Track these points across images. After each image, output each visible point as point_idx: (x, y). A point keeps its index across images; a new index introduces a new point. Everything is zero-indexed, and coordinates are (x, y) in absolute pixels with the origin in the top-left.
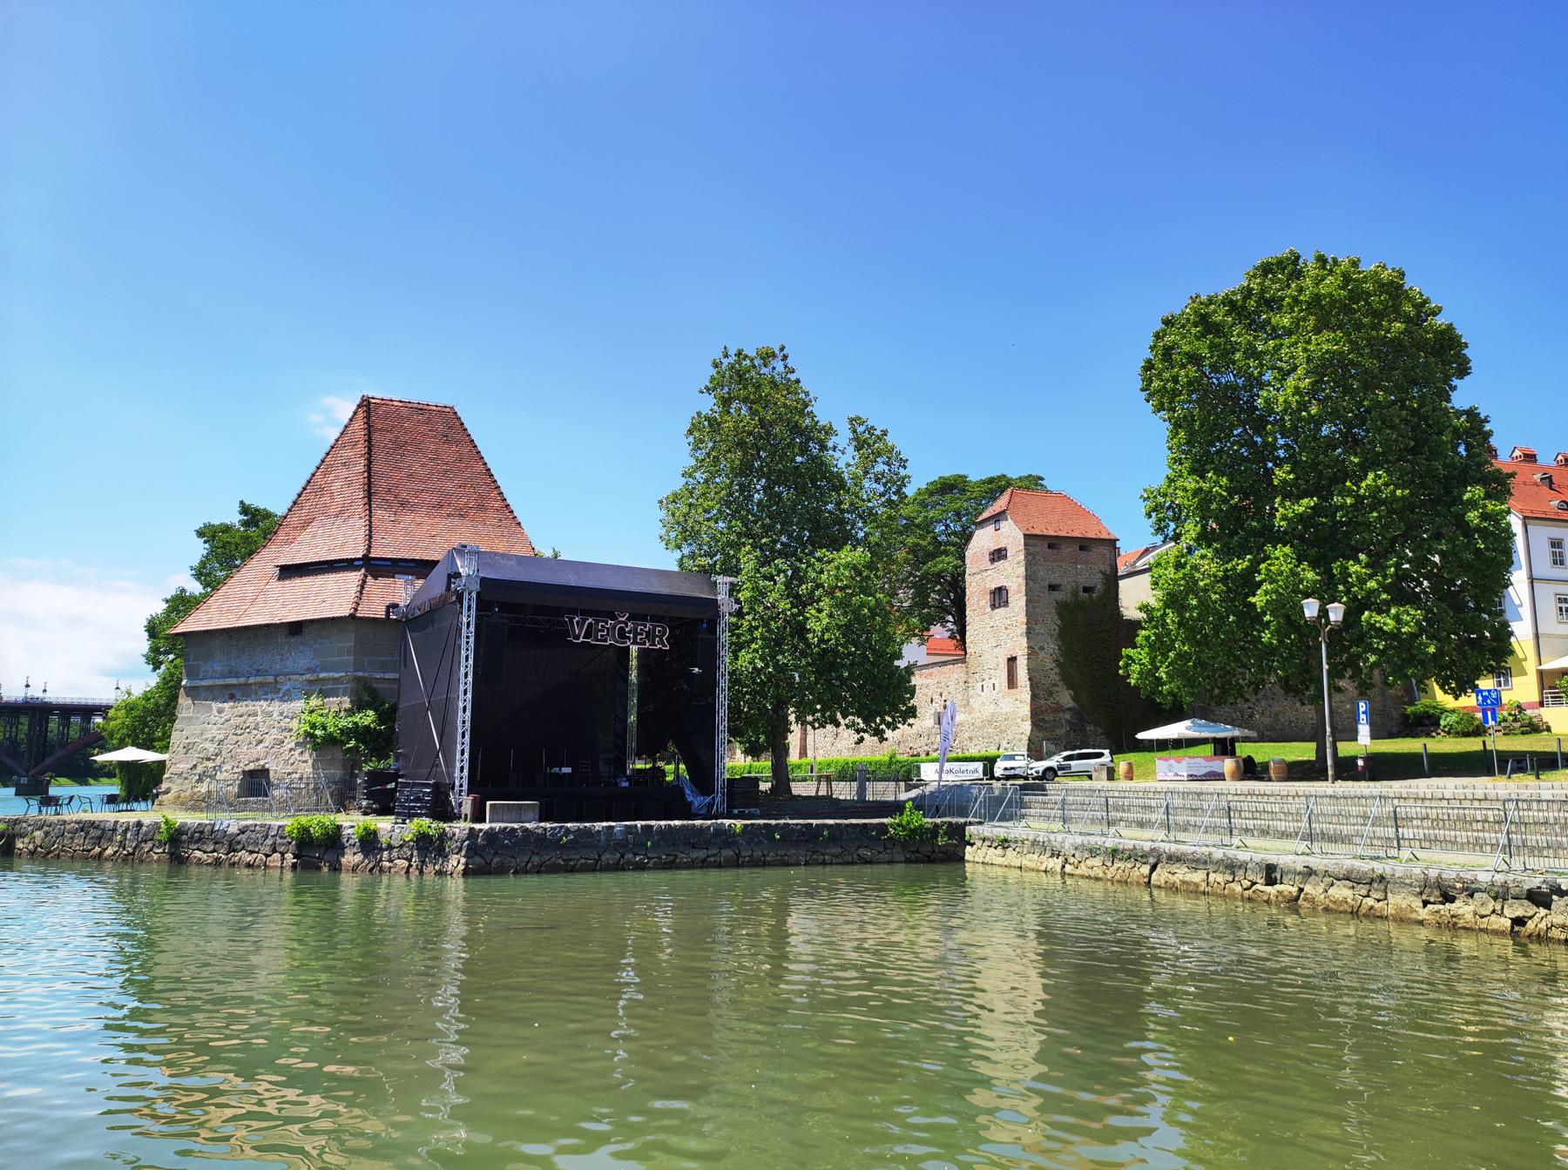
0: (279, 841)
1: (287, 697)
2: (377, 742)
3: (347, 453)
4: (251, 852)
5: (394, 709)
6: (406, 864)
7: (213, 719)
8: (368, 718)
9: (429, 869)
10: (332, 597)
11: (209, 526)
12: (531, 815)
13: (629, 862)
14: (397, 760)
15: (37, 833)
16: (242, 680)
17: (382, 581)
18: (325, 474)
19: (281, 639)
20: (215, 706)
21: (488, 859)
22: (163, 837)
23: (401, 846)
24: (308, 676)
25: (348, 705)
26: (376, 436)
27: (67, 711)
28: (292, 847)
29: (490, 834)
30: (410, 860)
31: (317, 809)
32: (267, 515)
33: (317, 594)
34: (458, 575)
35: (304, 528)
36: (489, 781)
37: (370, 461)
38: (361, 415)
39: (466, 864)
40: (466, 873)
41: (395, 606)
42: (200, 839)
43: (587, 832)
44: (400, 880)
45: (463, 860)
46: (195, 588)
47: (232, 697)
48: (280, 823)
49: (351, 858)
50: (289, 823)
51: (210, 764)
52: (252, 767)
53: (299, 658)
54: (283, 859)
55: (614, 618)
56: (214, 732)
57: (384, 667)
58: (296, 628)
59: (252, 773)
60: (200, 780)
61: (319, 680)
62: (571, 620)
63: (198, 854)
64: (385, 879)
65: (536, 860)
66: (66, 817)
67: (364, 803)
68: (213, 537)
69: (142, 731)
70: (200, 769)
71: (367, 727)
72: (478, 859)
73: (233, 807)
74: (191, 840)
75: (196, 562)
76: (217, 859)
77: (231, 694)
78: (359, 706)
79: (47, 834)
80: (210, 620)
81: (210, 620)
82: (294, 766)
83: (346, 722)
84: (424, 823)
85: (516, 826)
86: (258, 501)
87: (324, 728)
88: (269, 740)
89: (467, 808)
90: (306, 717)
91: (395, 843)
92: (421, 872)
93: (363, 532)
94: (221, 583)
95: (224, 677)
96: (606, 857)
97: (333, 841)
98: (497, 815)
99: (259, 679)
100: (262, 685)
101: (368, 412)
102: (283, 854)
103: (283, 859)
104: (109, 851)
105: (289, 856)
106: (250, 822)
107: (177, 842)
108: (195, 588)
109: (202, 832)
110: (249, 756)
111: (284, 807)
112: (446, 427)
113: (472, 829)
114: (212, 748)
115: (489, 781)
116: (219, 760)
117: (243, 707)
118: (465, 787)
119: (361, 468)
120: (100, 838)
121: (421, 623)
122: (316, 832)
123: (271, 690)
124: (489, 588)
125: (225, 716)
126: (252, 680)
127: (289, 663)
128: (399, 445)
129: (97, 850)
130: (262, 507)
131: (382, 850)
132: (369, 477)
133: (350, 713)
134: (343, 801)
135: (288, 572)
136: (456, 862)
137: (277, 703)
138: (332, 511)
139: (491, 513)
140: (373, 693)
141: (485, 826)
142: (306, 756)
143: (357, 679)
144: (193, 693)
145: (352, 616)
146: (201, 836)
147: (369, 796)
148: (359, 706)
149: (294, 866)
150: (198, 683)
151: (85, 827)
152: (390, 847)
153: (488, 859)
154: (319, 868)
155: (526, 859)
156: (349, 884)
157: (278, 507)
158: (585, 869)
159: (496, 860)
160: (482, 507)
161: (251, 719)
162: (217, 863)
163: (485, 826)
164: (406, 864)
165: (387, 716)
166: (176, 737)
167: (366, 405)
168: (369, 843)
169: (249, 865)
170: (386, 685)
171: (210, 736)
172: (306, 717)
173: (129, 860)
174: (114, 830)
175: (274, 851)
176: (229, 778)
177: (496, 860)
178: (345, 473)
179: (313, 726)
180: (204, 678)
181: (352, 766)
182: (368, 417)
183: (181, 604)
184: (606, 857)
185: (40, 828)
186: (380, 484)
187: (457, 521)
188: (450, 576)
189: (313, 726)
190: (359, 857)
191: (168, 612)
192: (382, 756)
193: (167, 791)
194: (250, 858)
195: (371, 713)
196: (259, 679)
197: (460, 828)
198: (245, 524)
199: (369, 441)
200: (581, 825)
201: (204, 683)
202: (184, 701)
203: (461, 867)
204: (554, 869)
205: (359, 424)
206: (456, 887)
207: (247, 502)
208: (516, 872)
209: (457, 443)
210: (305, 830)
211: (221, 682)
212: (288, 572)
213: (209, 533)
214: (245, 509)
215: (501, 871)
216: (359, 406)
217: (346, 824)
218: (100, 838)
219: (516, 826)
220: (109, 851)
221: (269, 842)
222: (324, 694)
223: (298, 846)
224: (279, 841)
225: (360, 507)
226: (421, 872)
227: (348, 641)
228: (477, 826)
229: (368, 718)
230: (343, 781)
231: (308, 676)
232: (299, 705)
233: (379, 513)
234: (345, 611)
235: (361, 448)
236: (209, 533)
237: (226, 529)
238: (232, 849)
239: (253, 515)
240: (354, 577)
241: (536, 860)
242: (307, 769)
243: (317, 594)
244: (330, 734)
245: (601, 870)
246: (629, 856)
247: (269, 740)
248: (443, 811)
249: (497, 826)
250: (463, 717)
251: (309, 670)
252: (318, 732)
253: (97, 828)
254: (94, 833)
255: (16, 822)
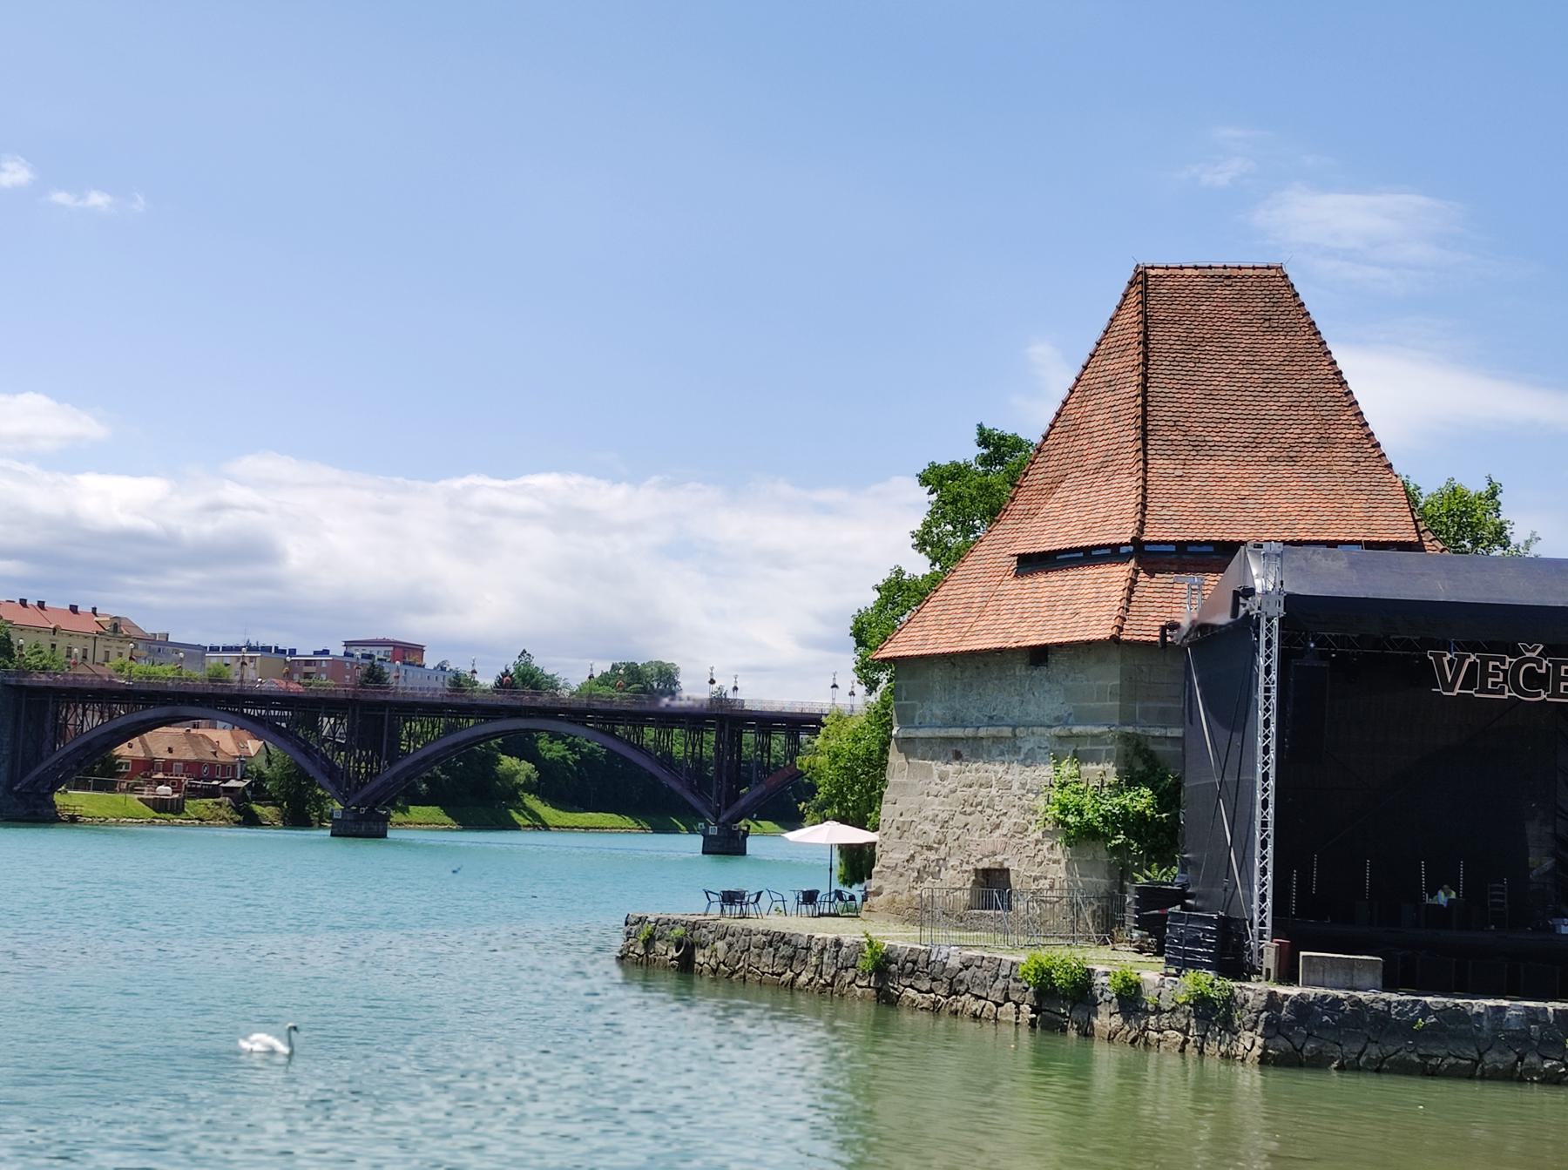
0: (1012, 984)
1: (1029, 760)
2: (1157, 837)
3: (1113, 365)
4: (978, 998)
5: (1178, 784)
6: (1181, 1038)
7: (934, 789)
8: (1141, 800)
9: (1212, 1048)
10: (1086, 607)
11: (934, 467)
12: (1368, 979)
13: (1532, 1070)
14: (1183, 870)
15: (719, 944)
16: (969, 732)
17: (1162, 579)
18: (1081, 402)
19: (1020, 670)
20: (937, 767)
21: (1298, 1042)
22: (865, 964)
23: (1173, 1010)
24: (1057, 730)
25: (1112, 778)
26: (1156, 334)
27: (767, 722)
28: (1030, 996)
29: (1300, 1005)
30: (1186, 1033)
31: (1071, 939)
32: (1018, 444)
33: (1067, 602)
34: (1249, 592)
35: (1052, 491)
36: (1307, 921)
37: (1146, 378)
38: (1134, 299)
39: (1265, 1048)
40: (1264, 1060)
41: (1174, 626)
42: (913, 972)
43: (1459, 1015)
44: (1173, 1060)
45: (1259, 1041)
46: (919, 566)
47: (958, 756)
48: (1014, 959)
49: (1106, 1020)
50: (1020, 955)
51: (932, 856)
52: (985, 864)
53: (1045, 700)
54: (1018, 1012)
55: (1515, 652)
56: (934, 807)
57: (1164, 718)
58: (1039, 655)
59: (986, 872)
60: (919, 879)
61: (1071, 736)
62: (1439, 658)
63: (911, 993)
64: (1153, 1055)
65: (1374, 1051)
66: (751, 924)
67: (1136, 934)
68: (941, 485)
69: (851, 789)
70: (919, 863)
71: (1141, 814)
72: (1282, 1042)
73: (961, 922)
74: (901, 971)
75: (917, 526)
76: (935, 1003)
77: (956, 750)
78: (1131, 779)
79: (730, 946)
80: (925, 639)
81: (925, 639)
82: (1044, 869)
83: (1112, 804)
84: (1202, 980)
85: (1341, 994)
86: (1004, 425)
87: (1080, 814)
88: (1007, 823)
89: (1270, 961)
90: (1056, 795)
91: (1165, 1005)
92: (1201, 1052)
93: (1134, 497)
94: (959, 556)
95: (946, 725)
96: (1491, 1058)
97: (1081, 992)
98: (1318, 974)
99: (992, 731)
100: (997, 739)
101: (1145, 293)
102: (1017, 1005)
103: (1018, 1012)
104: (803, 979)
105: (1025, 1008)
106: (976, 953)
107: (885, 971)
108: (919, 566)
109: (915, 962)
110: (986, 848)
111: (1033, 927)
112: (1265, 309)
113: (1272, 994)
114: (933, 833)
115: (1307, 921)
116: (943, 850)
117: (976, 770)
118: (1269, 927)
119: (1133, 390)
120: (792, 958)
121: (1217, 650)
122: (1060, 978)
123: (1008, 748)
124: (1299, 610)
125: (950, 784)
126: (982, 732)
127: (1031, 708)
128: (1192, 346)
129: (789, 974)
130: (1009, 432)
131: (1147, 1012)
132: (1144, 405)
133: (1117, 789)
134: (1107, 928)
135: (1030, 564)
136: (1250, 1042)
137: (1016, 768)
138: (1090, 464)
139: (1341, 451)
140: (1150, 759)
141: (1294, 991)
142: (1058, 854)
143: (1126, 738)
144: (907, 746)
145: (1115, 639)
146: (916, 967)
147: (1142, 924)
148: (1131, 779)
149: (1032, 1023)
150: (913, 733)
151: (775, 940)
152: (1158, 1011)
153: (1298, 1042)
154: (1064, 1030)
155: (1357, 1048)
156: (1105, 1058)
157: (1032, 432)
158: (1455, 1073)
159: (1310, 1045)
160: (1326, 442)
161: (983, 791)
162: (935, 1009)
163: (1294, 991)
164: (1181, 1038)
165: (1168, 798)
166: (887, 811)
167: (1142, 280)
168: (1130, 999)
169: (975, 1017)
170: (1168, 748)
171: (930, 813)
172: (1056, 795)
173: (827, 990)
174: (808, 949)
175: (1007, 999)
176: (956, 881)
177: (1310, 1045)
178: (1109, 399)
179: (1064, 809)
180: (921, 726)
181: (1122, 874)
182: (1144, 303)
183: (900, 595)
184: (1491, 1058)
185: (723, 938)
186: (1161, 414)
187: (1282, 469)
188: (1236, 594)
189: (1064, 809)
190: (1117, 1020)
191: (881, 607)
192: (1166, 861)
193: (878, 893)
194: (976, 1006)
195: (1146, 792)
196: (992, 731)
197: (1255, 990)
198: (985, 461)
199: (1145, 343)
200: (1449, 1002)
201: (922, 733)
202: (895, 758)
203: (1257, 1051)
204: (1404, 1069)
205: (1131, 315)
206: (1249, 1078)
207: (987, 427)
208: (1341, 1068)
209: (1288, 329)
210: (1044, 973)
211: (943, 733)
212: (1030, 564)
213: (935, 478)
214: (985, 438)
215: (1318, 1063)
216: (1131, 284)
217: (1100, 969)
218: (792, 958)
219: (1341, 994)
220: (803, 979)
221: (1000, 984)
222: (1080, 758)
223: (1037, 995)
224: (1012, 984)
225: (1130, 456)
226: (1201, 1052)
227: (1108, 677)
228: (1282, 990)
229: (1141, 800)
230: (1110, 896)
231: (1057, 730)
232: (1045, 772)
233: (1158, 464)
234: (1103, 632)
235: (1134, 357)
236: (935, 478)
237: (957, 472)
238: (953, 992)
239: (997, 447)
240: (1120, 573)
241: (1374, 1051)
242: (1059, 872)
243: (1067, 602)
244: (1088, 823)
245: (1482, 1078)
246: (1532, 1059)
247: (1007, 823)
248: (1234, 964)
249: (1311, 992)
250: (1264, 816)
251: (1059, 720)
252: (1070, 819)
253: (788, 943)
254: (785, 950)
255: (695, 926)
